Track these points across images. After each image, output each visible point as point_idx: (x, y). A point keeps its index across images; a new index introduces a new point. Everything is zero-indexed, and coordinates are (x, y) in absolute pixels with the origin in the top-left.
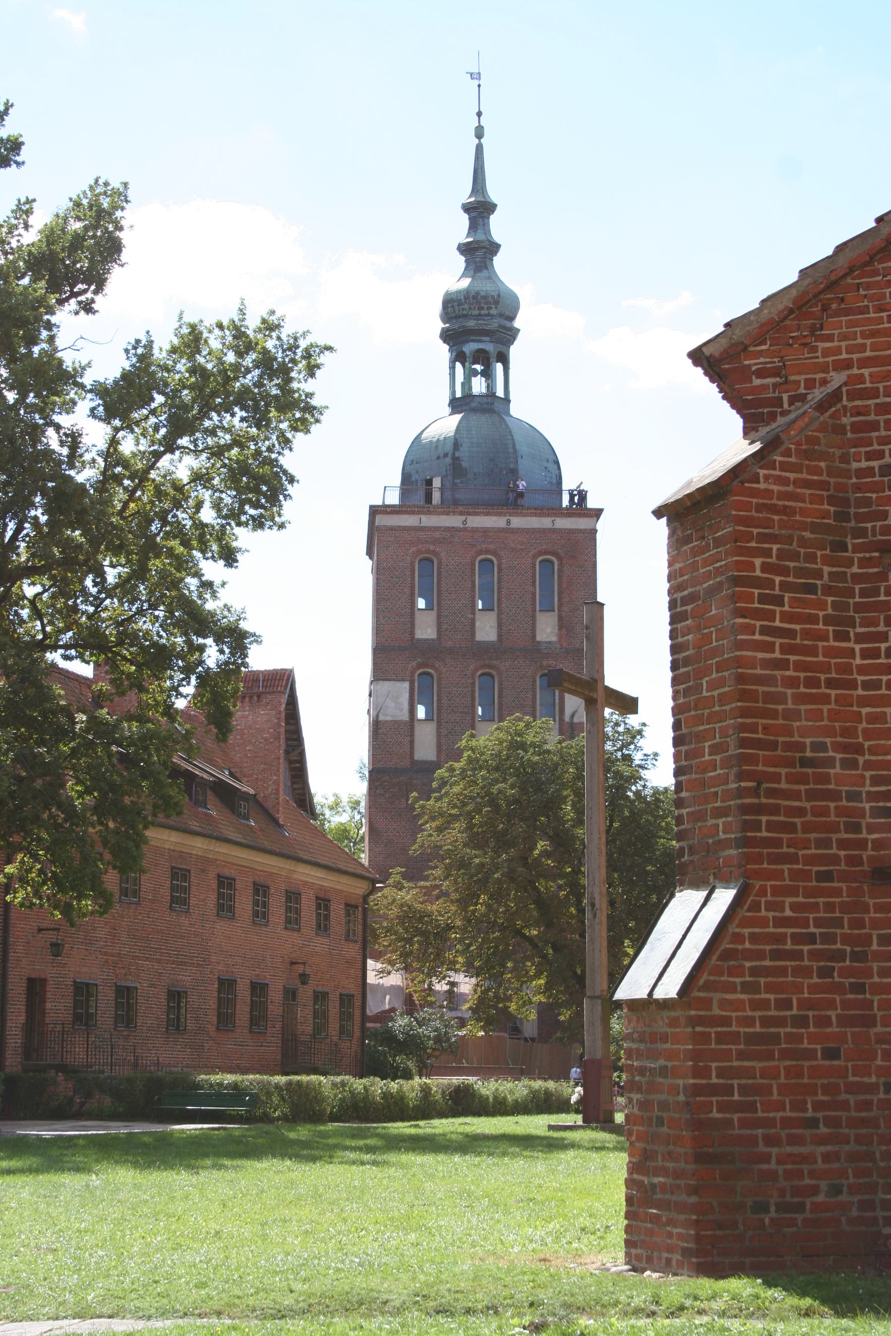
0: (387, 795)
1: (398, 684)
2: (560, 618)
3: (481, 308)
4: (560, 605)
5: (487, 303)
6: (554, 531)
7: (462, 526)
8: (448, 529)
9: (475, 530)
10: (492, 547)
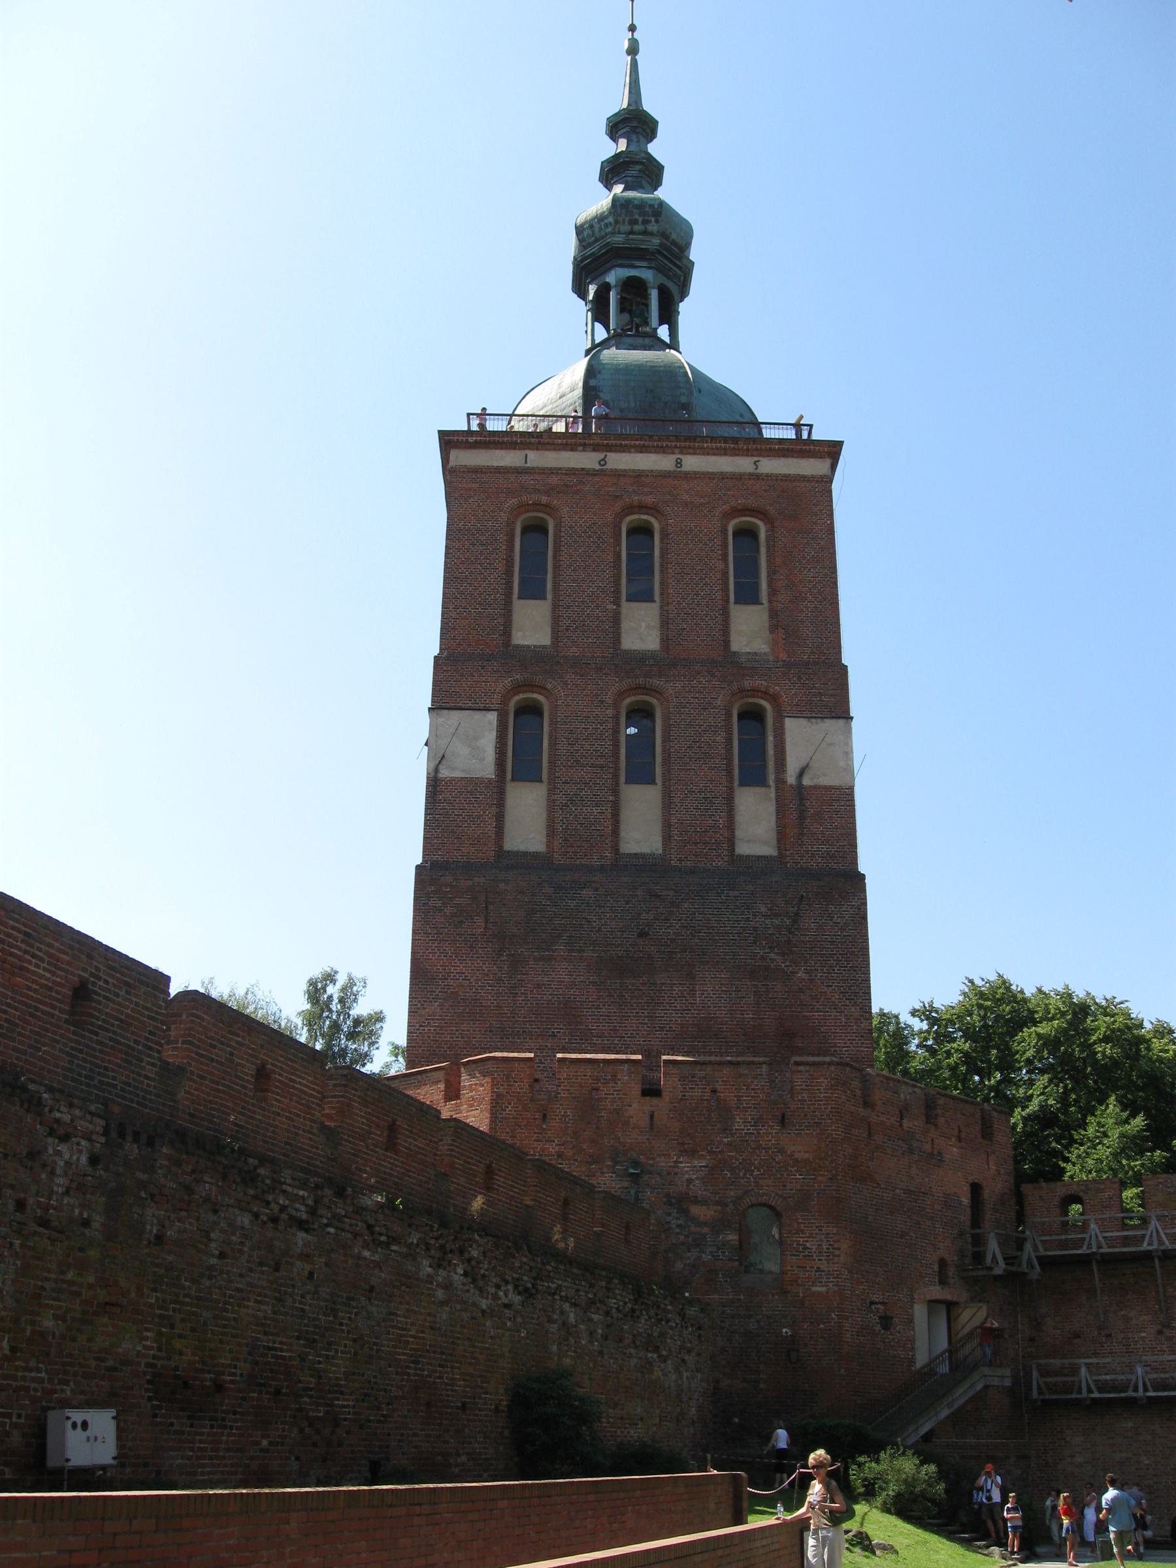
0: (448, 911)
1: (478, 715)
2: (773, 614)
3: (633, 222)
4: (773, 593)
5: (642, 214)
6: (757, 477)
7: (598, 467)
8: (572, 472)
9: (618, 474)
10: (650, 500)
